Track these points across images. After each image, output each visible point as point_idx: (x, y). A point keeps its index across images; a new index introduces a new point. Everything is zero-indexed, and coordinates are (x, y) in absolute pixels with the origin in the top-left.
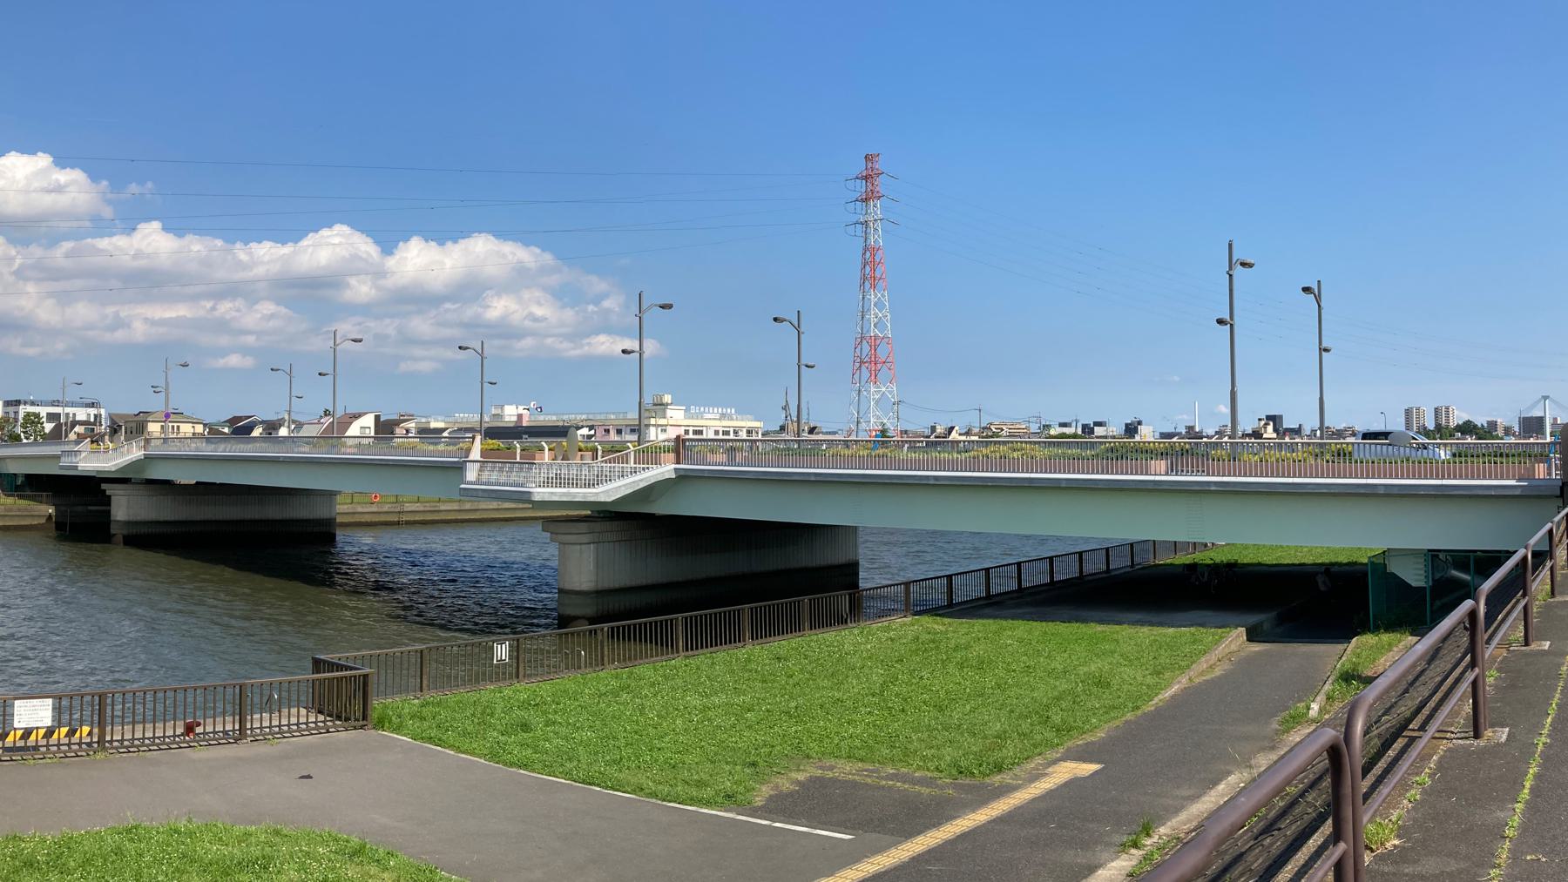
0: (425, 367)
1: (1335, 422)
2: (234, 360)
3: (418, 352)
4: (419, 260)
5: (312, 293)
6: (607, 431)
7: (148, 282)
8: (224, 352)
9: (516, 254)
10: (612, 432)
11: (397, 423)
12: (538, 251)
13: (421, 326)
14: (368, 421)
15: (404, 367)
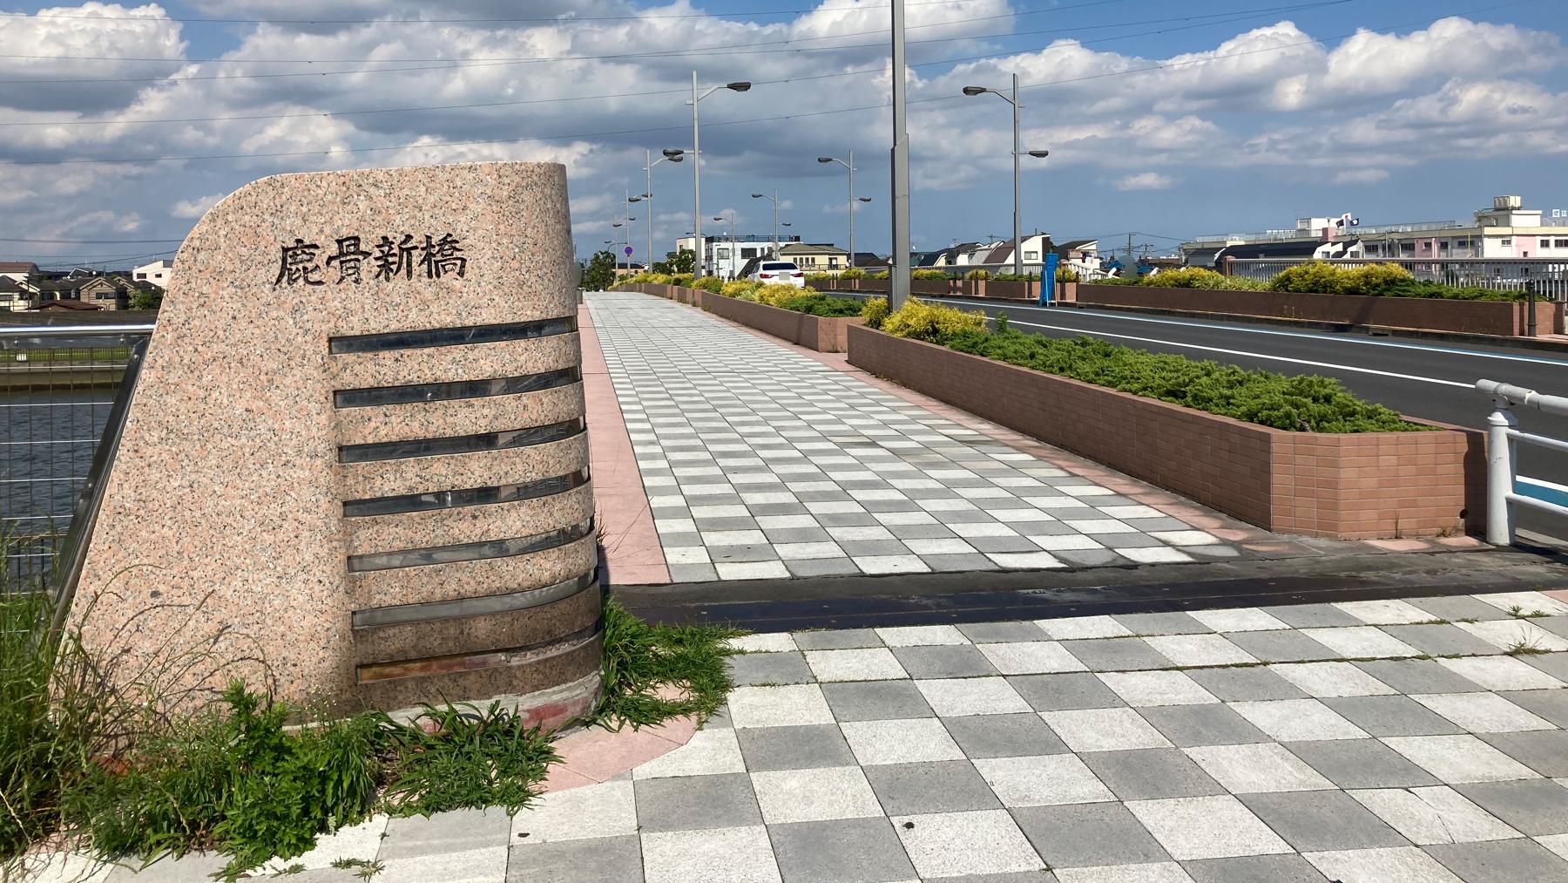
0: (1367, 176)
1: (1486, 240)
2: (1149, 180)
3: (1361, 160)
4: (1368, 56)
5: (1238, 103)
6: (1428, 245)
7: (1057, 100)
8: (1135, 172)
9: (1499, 37)
10: (1435, 247)
11: (1073, 246)
12: (1533, 33)
13: (1363, 131)
14: (1035, 244)
15: (1343, 177)
